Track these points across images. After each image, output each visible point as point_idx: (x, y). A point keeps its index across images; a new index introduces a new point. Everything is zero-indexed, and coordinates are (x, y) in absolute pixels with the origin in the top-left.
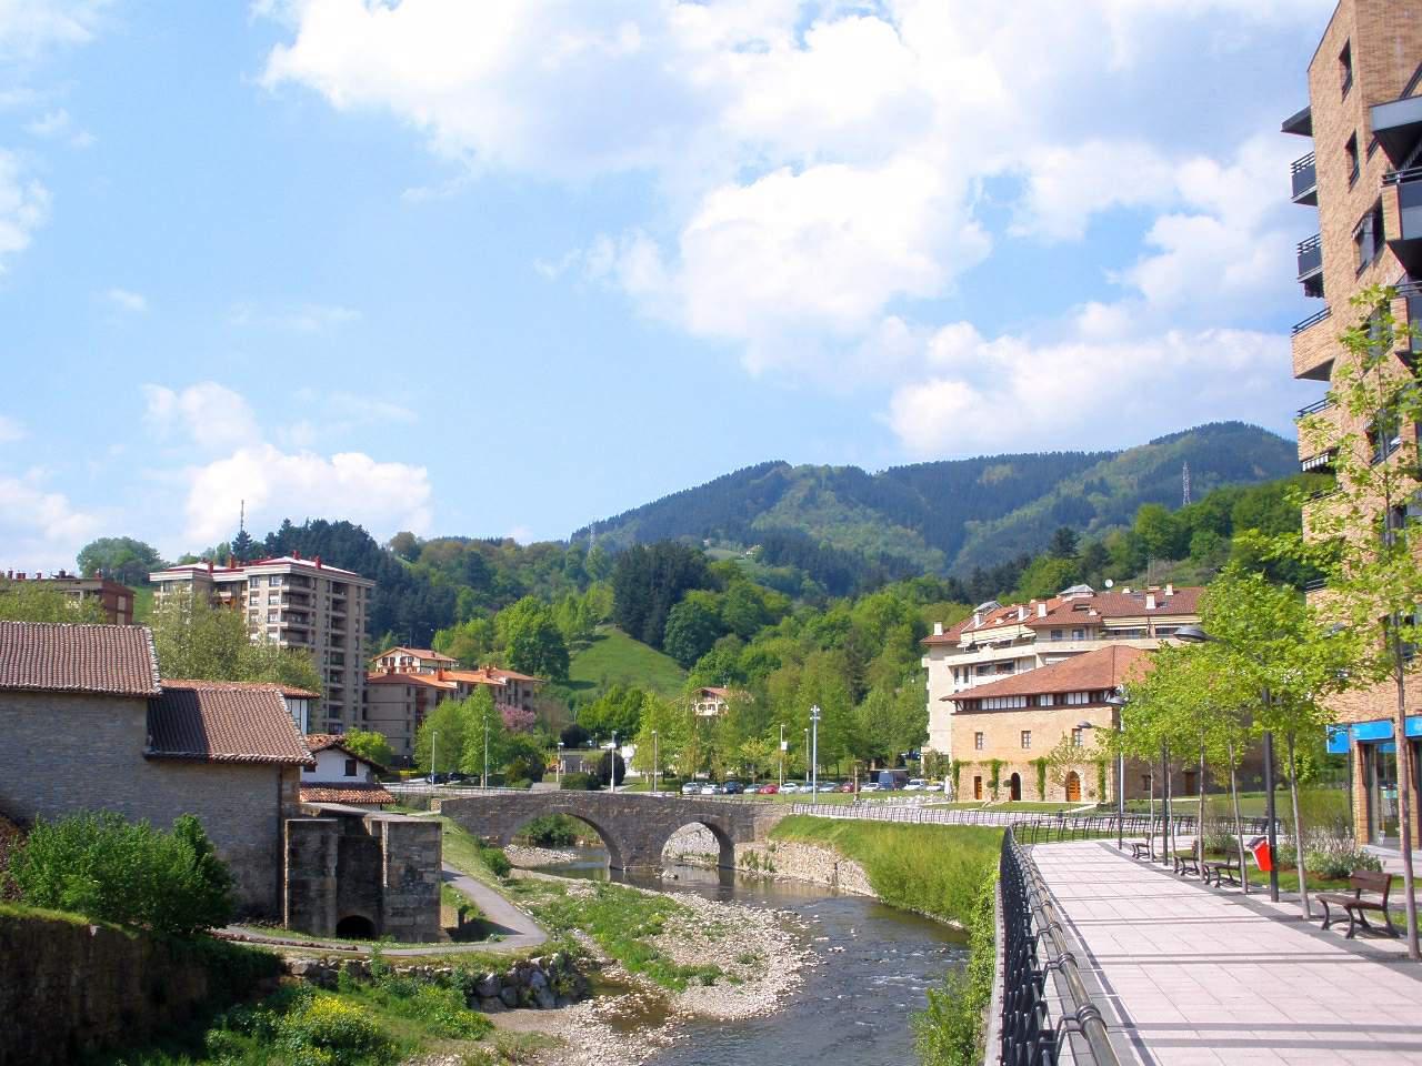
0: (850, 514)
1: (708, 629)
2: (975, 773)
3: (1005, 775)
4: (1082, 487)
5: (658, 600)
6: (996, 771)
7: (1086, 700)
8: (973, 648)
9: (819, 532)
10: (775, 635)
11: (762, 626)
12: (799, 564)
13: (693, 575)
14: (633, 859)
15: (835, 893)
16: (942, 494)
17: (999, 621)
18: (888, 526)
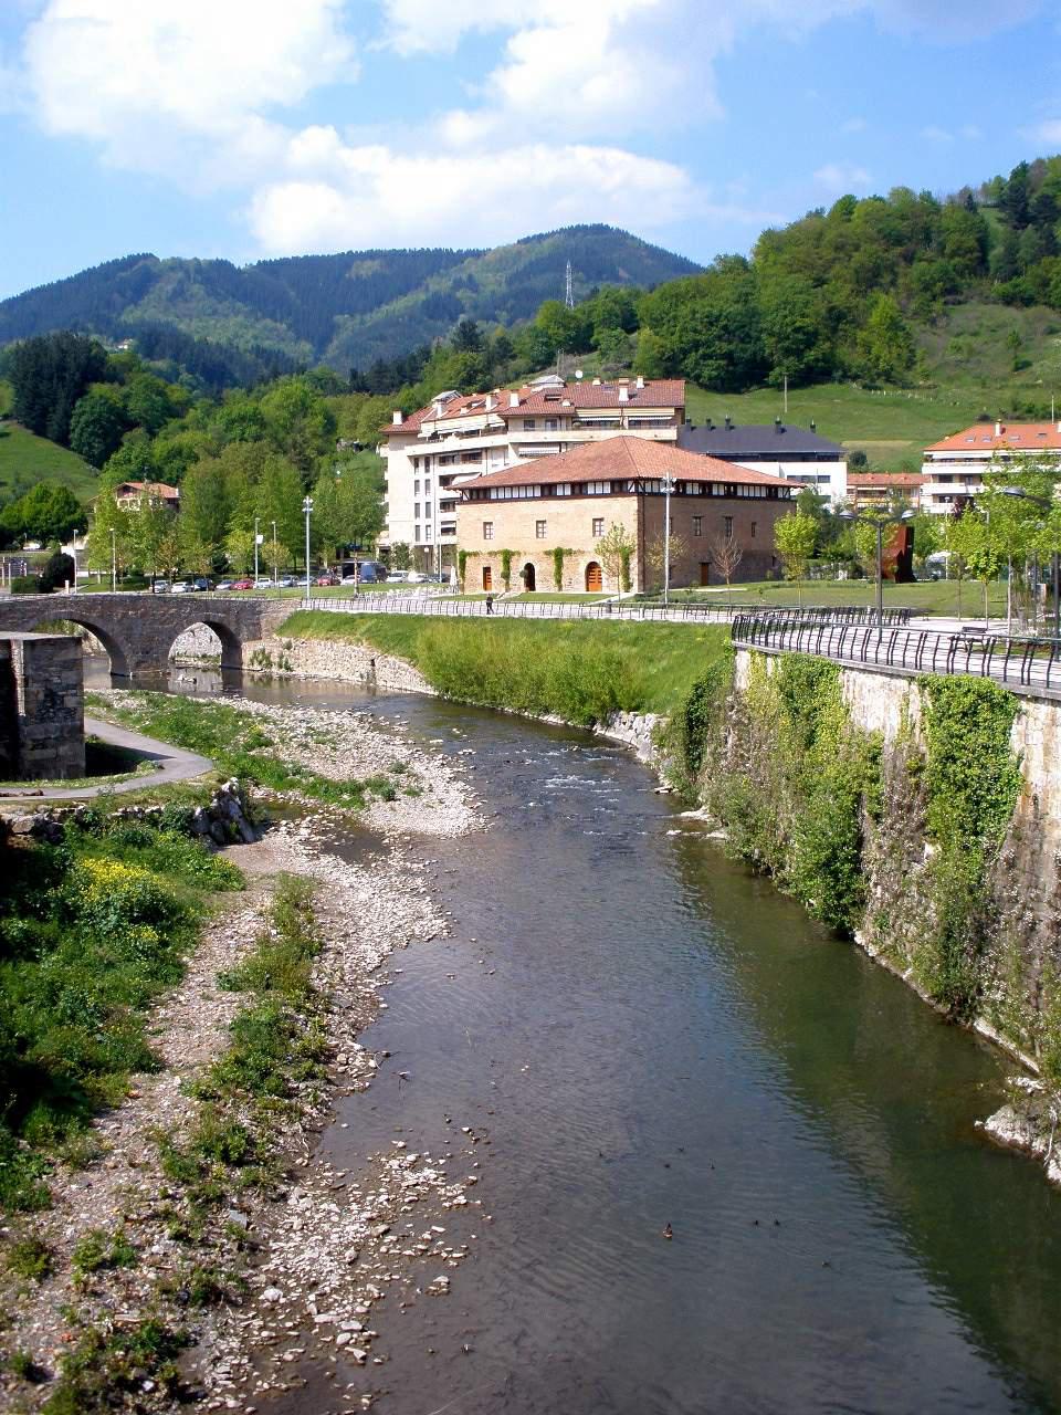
0: (220, 307)
1: (113, 423)
3: (518, 566)
4: (450, 283)
5: (62, 394)
6: (507, 562)
7: (538, 494)
8: (435, 437)
9: (189, 325)
10: (184, 428)
11: (168, 420)
12: (176, 358)
13: (95, 369)
14: (138, 664)
15: (372, 691)
16: (311, 288)
17: (464, 411)
18: (257, 320)
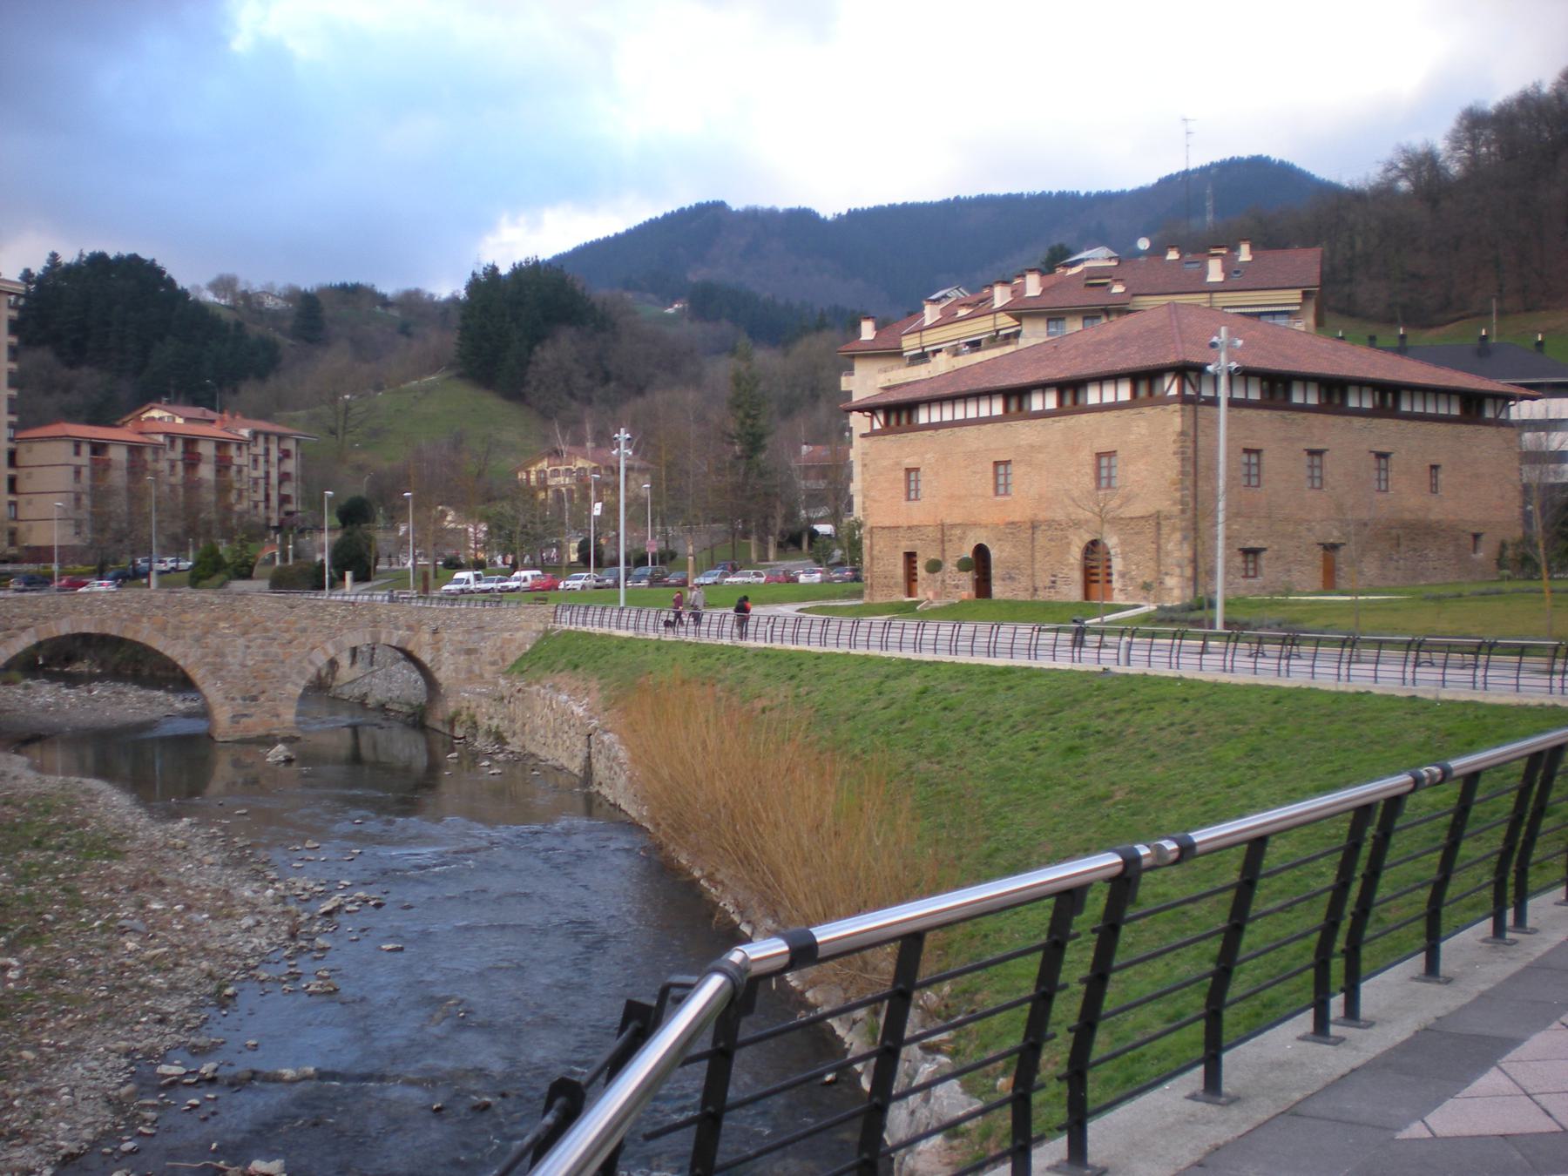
2: (905, 546)
